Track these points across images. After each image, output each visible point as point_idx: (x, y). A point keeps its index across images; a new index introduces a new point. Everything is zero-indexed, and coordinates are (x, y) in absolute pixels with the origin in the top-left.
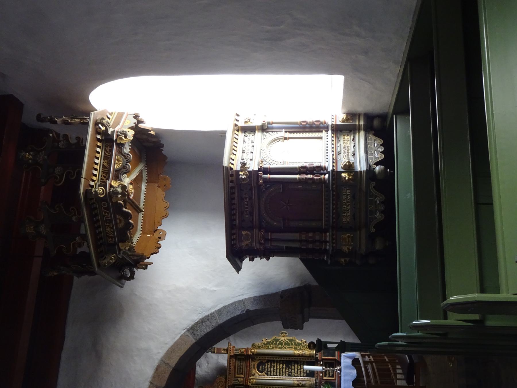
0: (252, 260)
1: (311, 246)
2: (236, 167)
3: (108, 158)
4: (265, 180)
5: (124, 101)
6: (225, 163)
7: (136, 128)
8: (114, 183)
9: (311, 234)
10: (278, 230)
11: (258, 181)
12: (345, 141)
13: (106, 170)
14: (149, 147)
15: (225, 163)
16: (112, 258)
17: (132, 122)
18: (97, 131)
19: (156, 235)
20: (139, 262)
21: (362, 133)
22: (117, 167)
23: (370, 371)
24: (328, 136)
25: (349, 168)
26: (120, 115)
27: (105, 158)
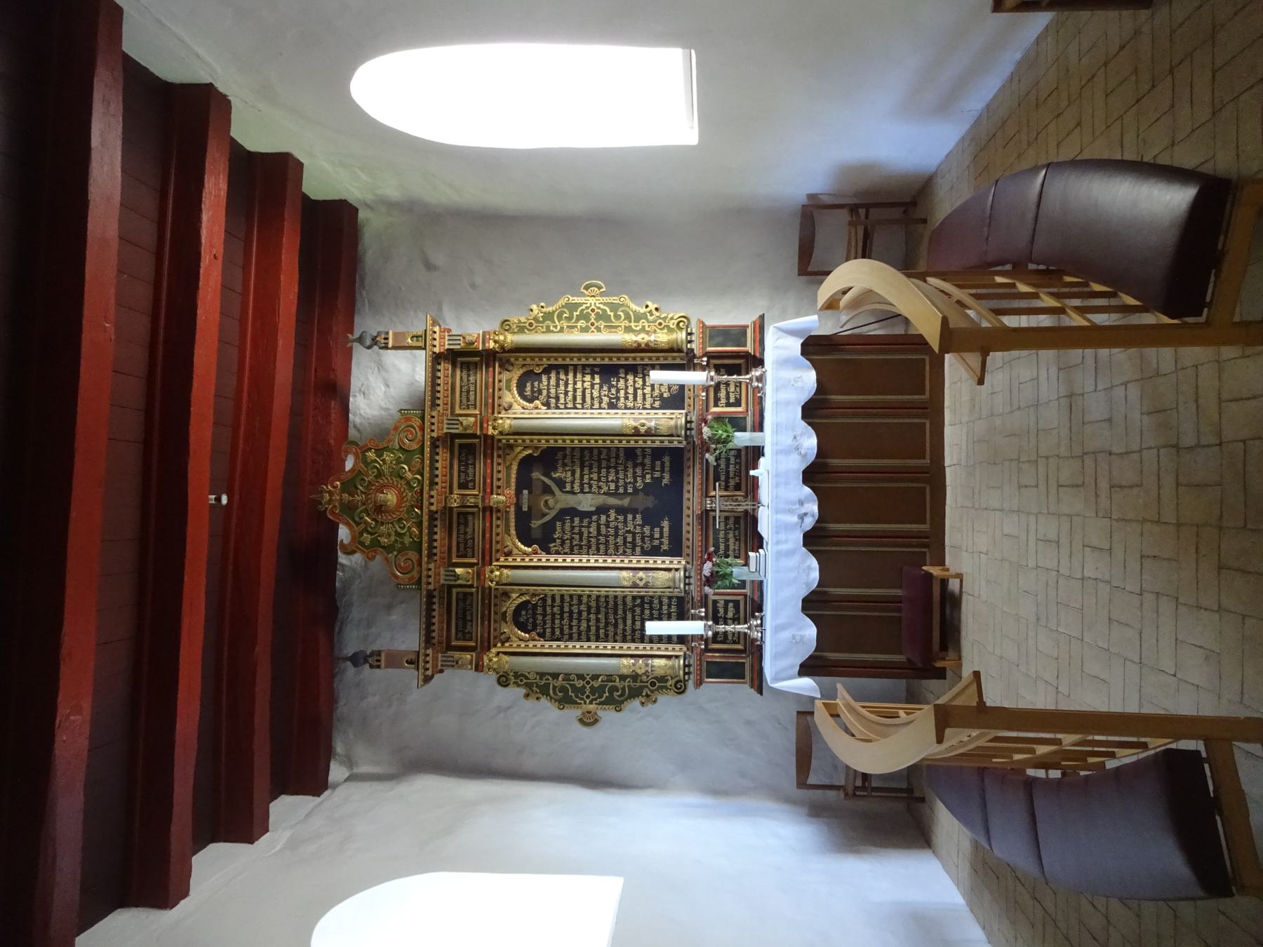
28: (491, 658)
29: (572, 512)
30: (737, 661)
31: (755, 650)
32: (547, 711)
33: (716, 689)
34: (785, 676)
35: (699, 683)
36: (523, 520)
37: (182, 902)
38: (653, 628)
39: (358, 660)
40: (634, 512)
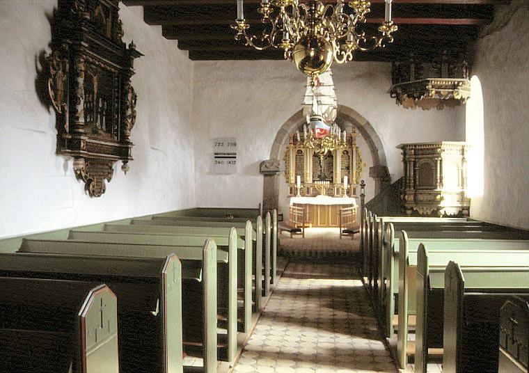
0: (54, 10)
1: (408, 181)
2: (443, 147)
3: (446, 87)
4: (437, 161)
5: (472, 90)
6: (443, 143)
7: (462, 99)
8: (433, 92)
9: (413, 181)
10: (415, 166)
11: (436, 157)
12: (457, 197)
13: (440, 87)
14: (455, 105)
15: (443, 143)
16: (399, 91)
17: (465, 96)
18: (459, 82)
19: (413, 105)
20: (399, 101)
21: (460, 205)
22: (442, 93)
23: (346, 212)
24: (460, 190)
25: (442, 199)
26: (469, 90)
27: (446, 86)
31: (295, 195)
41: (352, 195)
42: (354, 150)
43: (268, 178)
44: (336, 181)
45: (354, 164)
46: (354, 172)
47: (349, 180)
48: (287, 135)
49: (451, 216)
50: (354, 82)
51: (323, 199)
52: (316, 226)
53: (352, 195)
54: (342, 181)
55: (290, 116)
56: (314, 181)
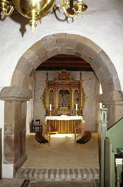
28: (47, 88)
29: (63, 96)
30: (47, 114)
31: (49, 115)
32: (42, 94)
33: (45, 111)
34: (48, 118)
35: (45, 110)
36: (62, 91)
37: (106, 53)
38: (51, 105)
39: (81, 74)
40: (63, 102)
41: (80, 114)
42: (81, 89)
43: (9, 103)
44: (71, 107)
45: (81, 98)
46: (81, 102)
47: (78, 106)
48: (82, 120)
49: (21, 98)
50: (89, 16)
51: (64, 118)
52: (61, 133)
53: (80, 114)
54: (75, 107)
55: (30, 46)
56: (59, 107)
